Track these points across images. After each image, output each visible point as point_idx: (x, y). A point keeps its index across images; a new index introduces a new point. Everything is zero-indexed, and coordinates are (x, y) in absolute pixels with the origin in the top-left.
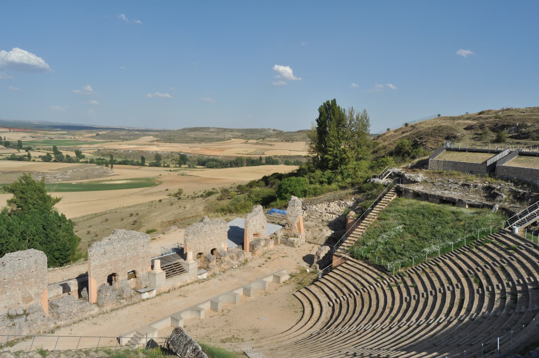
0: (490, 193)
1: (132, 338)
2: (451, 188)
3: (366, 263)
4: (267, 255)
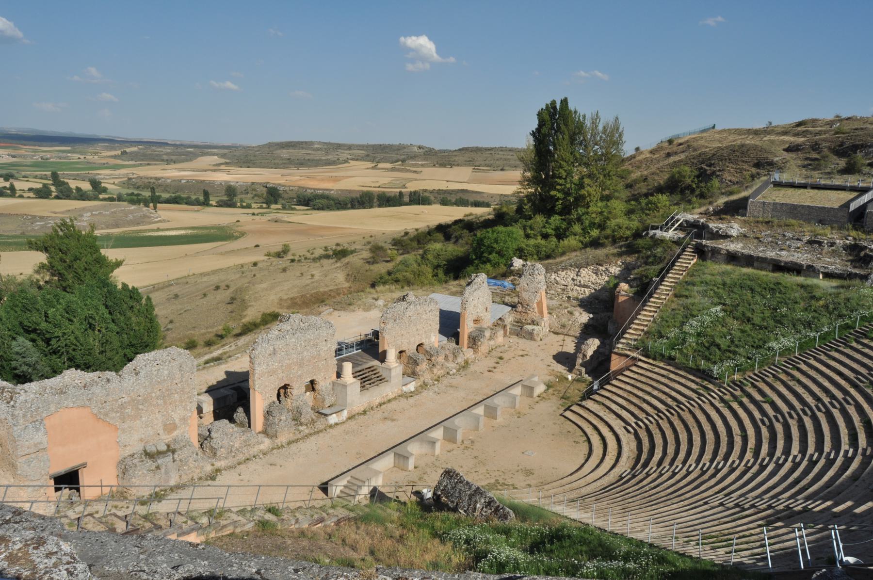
0: (858, 255)
1: (345, 487)
2: (790, 246)
3: (669, 365)
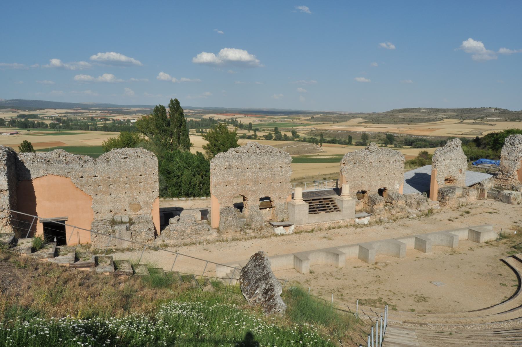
4: (464, 209)
